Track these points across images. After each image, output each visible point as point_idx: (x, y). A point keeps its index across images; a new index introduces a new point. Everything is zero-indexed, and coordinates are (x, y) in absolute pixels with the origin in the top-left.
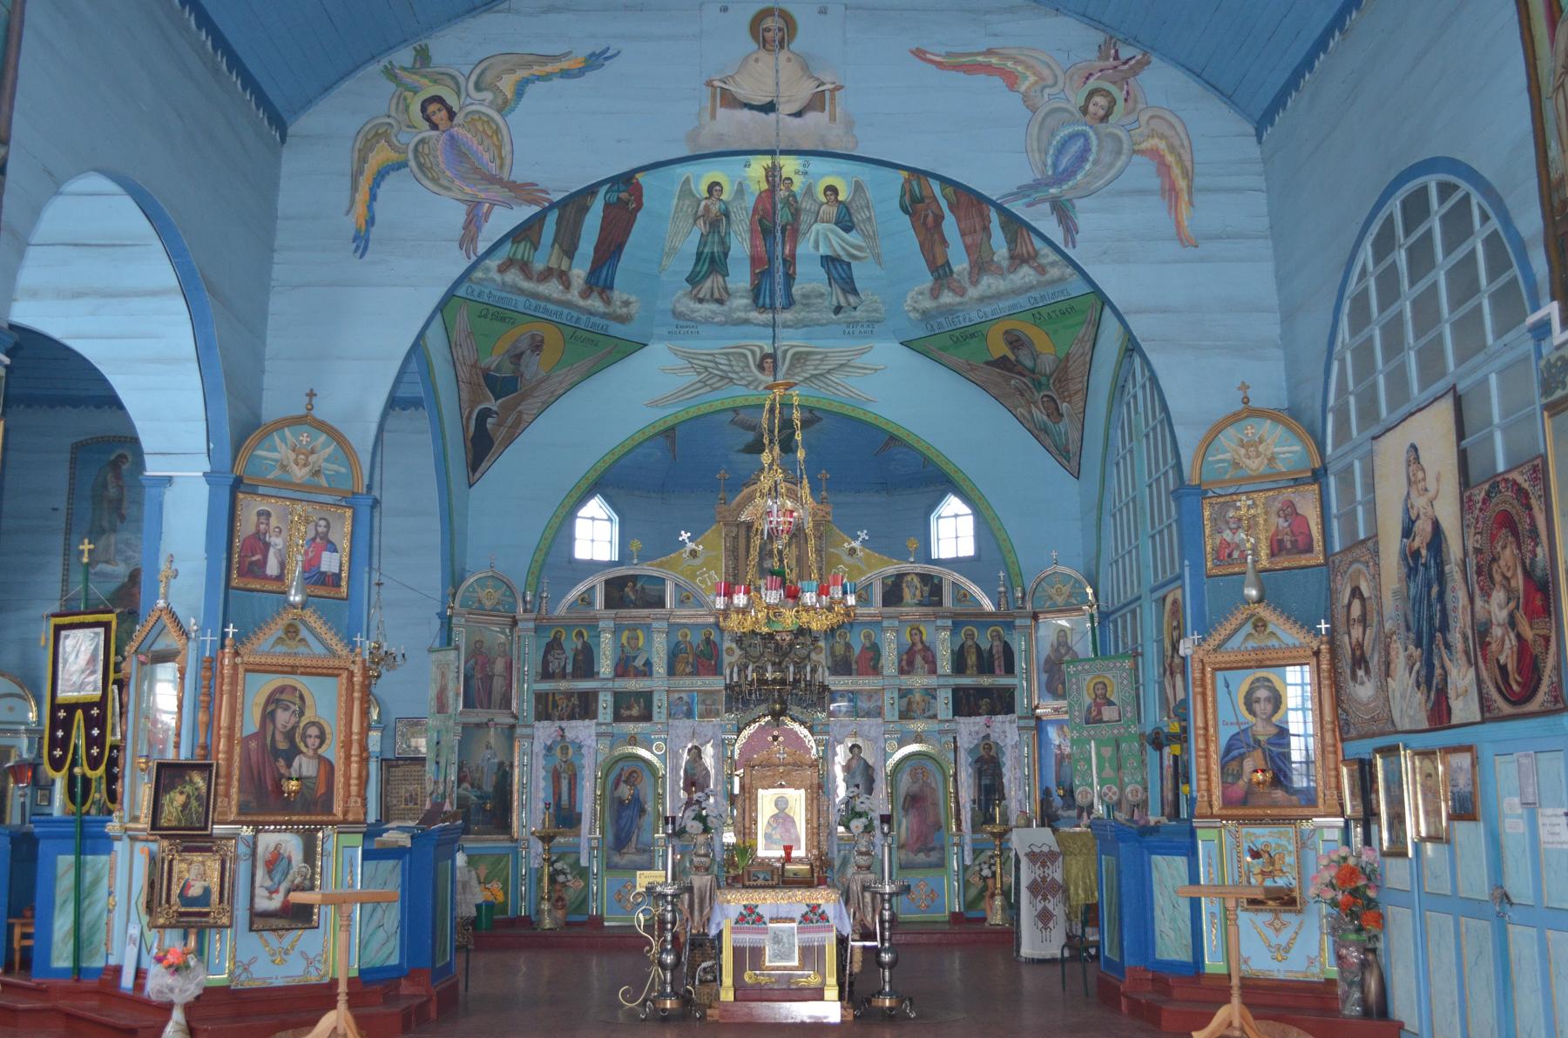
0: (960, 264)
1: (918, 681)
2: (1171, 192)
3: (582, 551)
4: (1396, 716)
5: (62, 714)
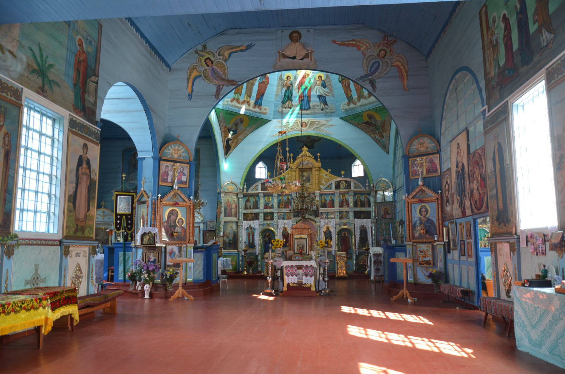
0: (355, 96)
1: (345, 209)
2: (402, 77)
3: (257, 176)
4: (454, 215)
5: (119, 217)
